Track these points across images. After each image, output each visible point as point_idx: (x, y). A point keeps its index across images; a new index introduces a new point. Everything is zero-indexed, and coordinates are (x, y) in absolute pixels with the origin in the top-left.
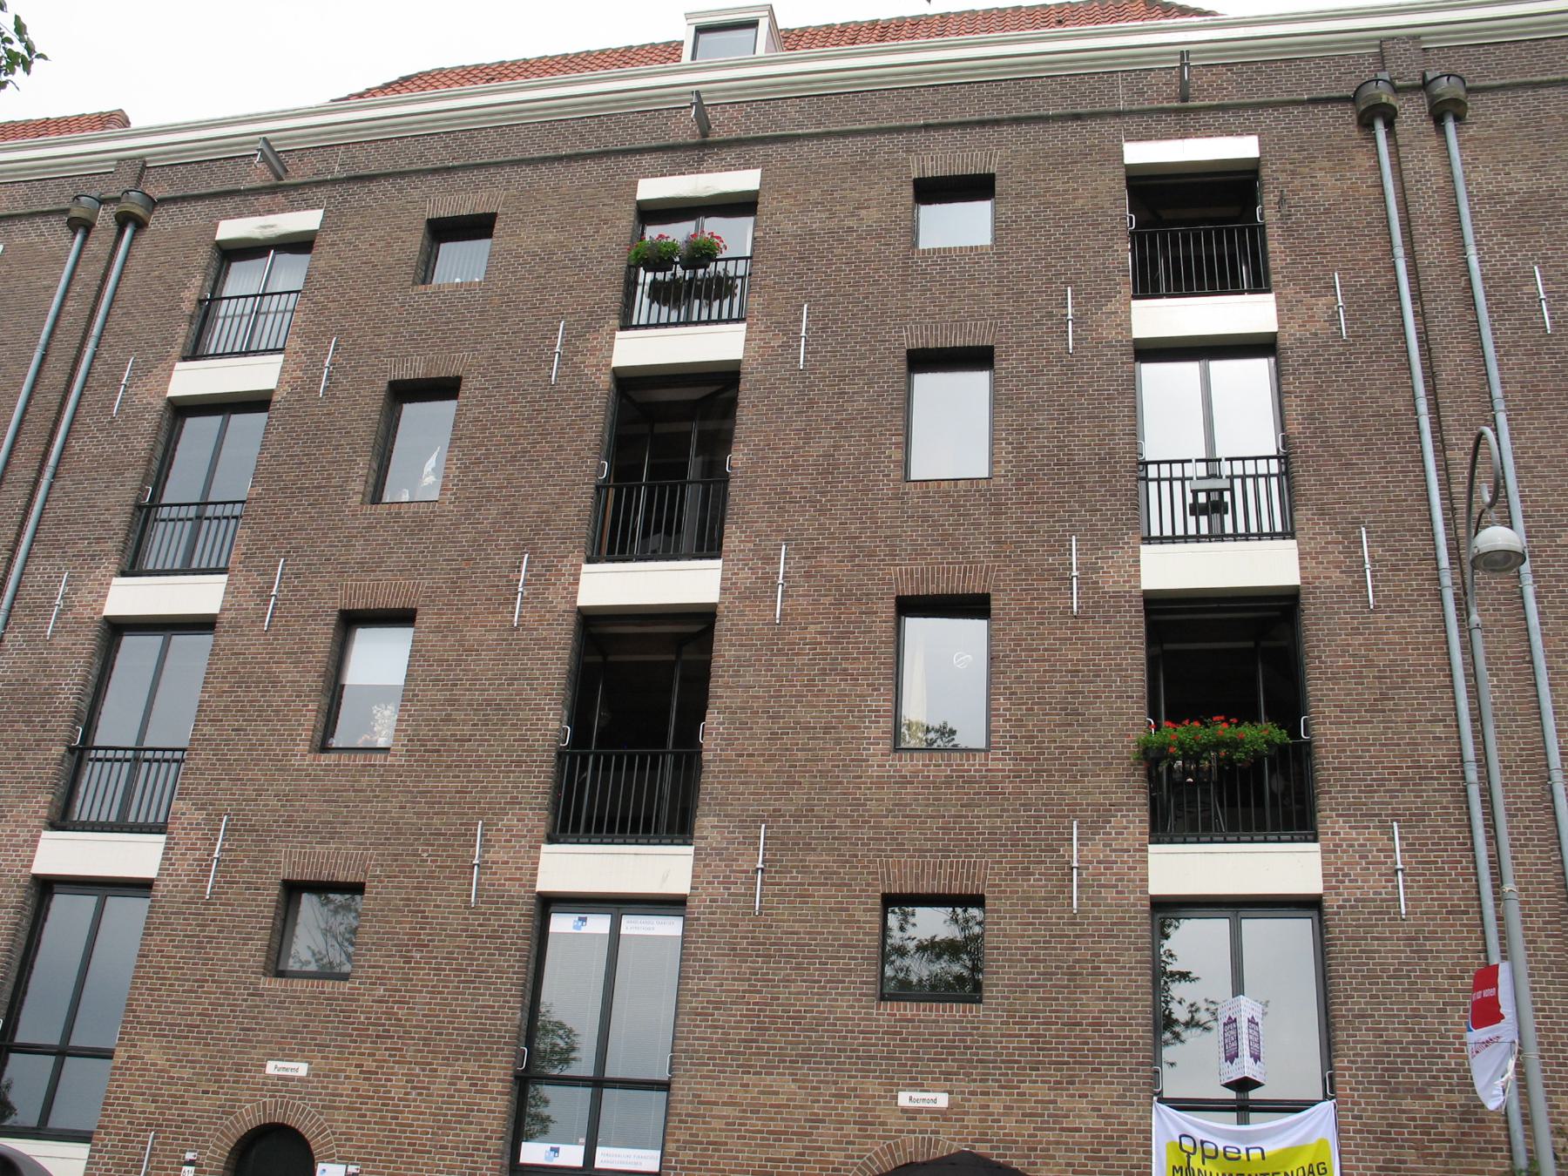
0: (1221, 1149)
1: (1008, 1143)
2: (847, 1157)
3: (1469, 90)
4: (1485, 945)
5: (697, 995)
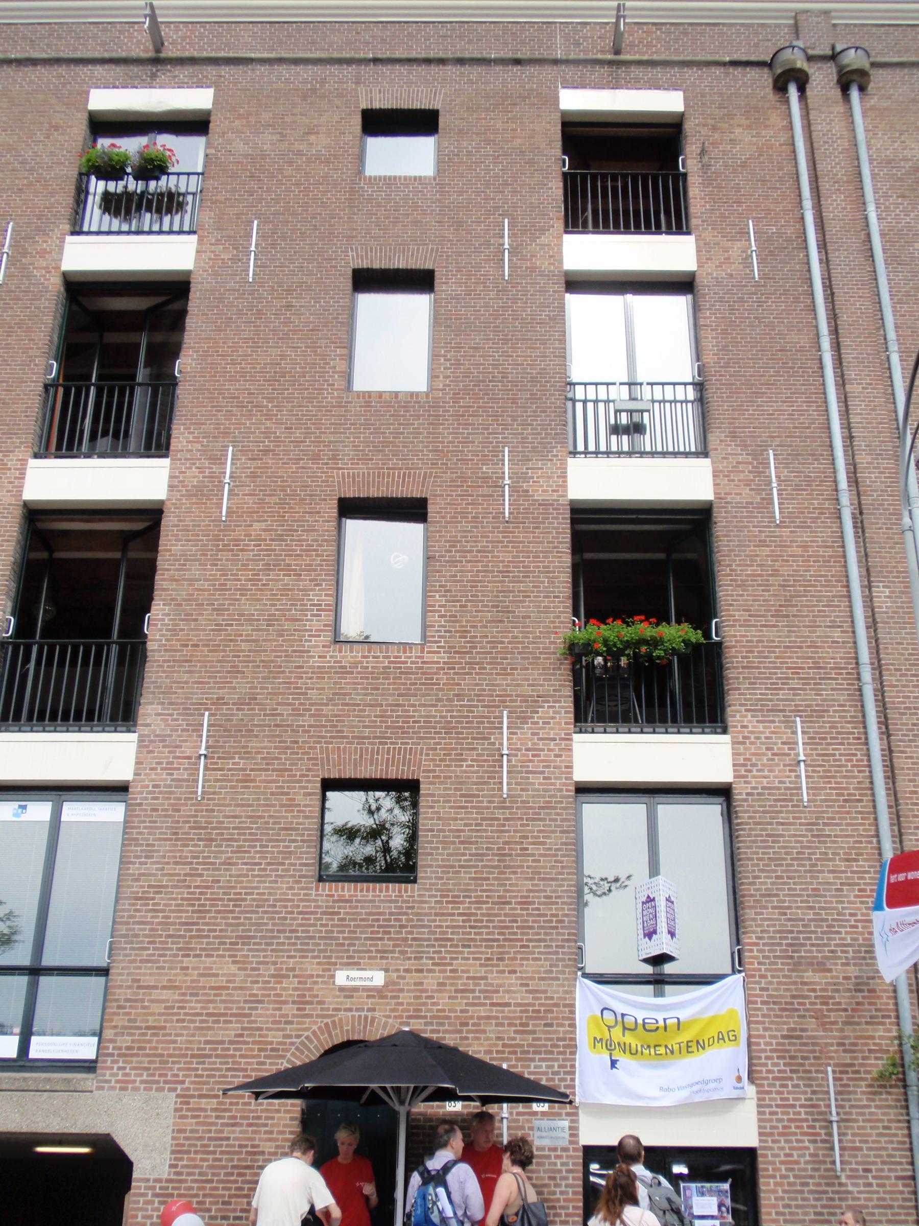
0: (640, 1021)
1: (441, 1018)
2: (285, 1036)
3: (874, 65)
4: (877, 830)
5: (137, 880)
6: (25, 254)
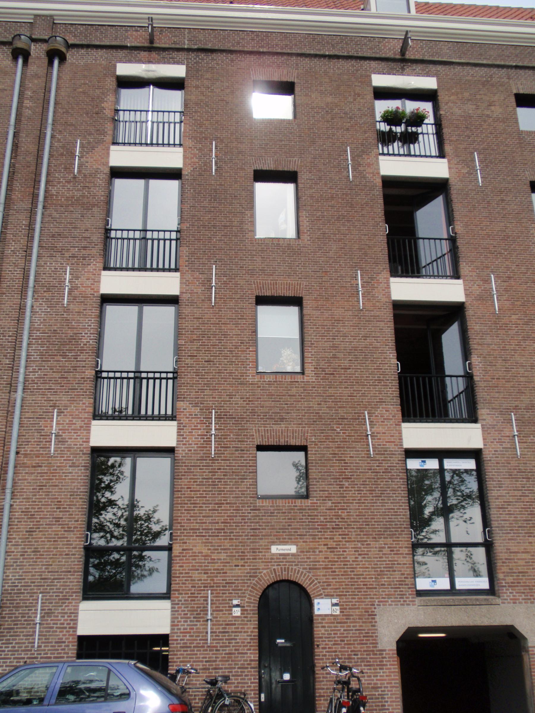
5: (497, 499)
6: (359, 165)
